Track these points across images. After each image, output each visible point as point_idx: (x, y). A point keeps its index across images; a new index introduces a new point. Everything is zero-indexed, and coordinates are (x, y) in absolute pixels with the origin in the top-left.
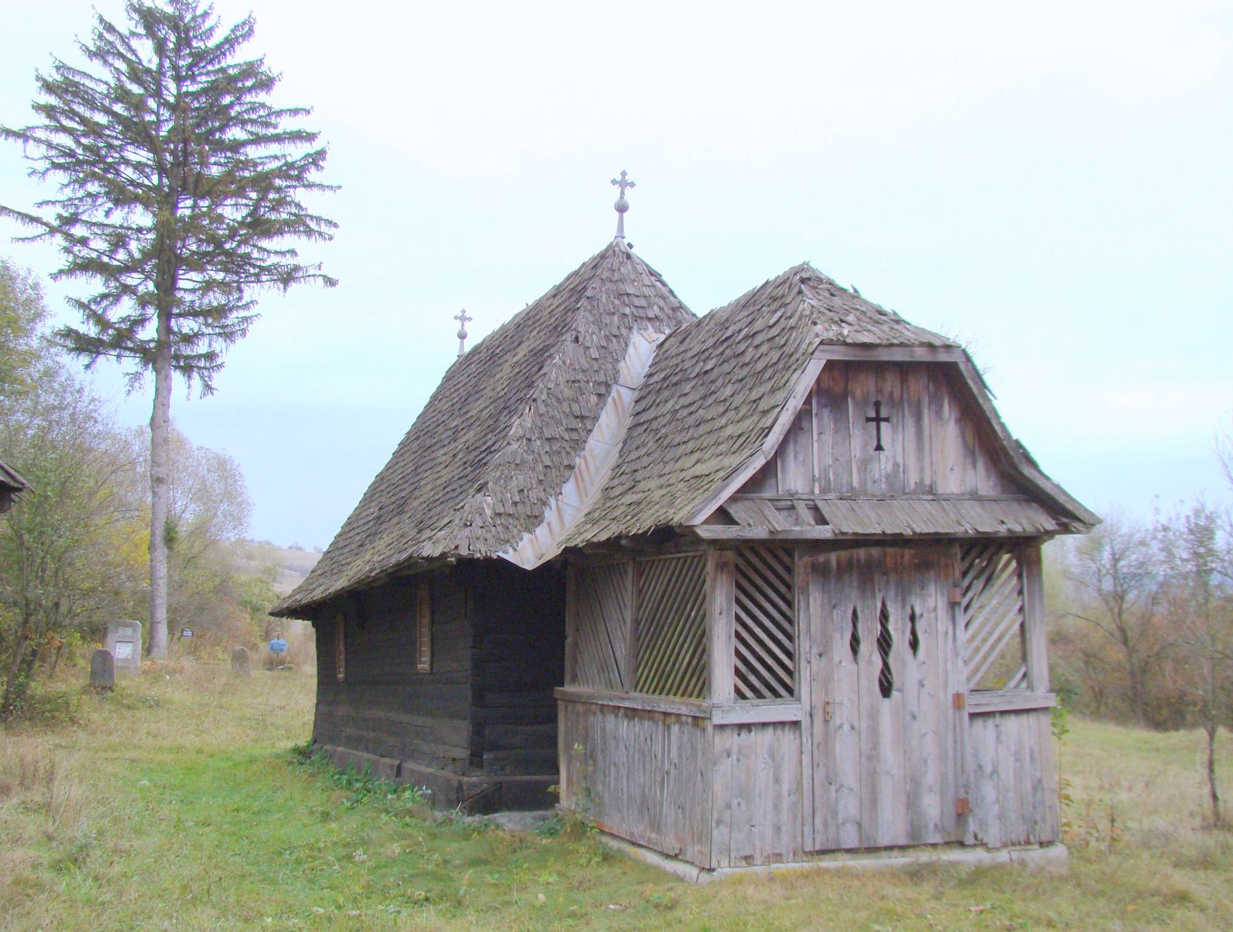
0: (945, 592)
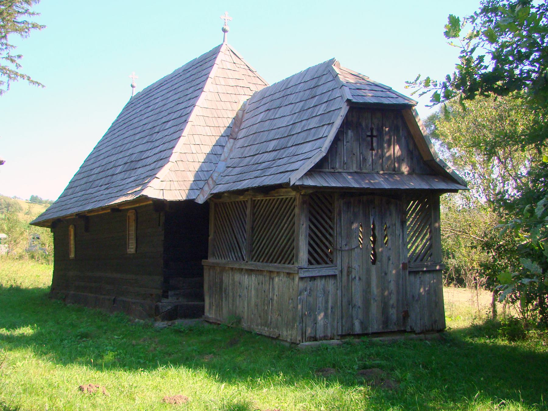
0: (399, 216)
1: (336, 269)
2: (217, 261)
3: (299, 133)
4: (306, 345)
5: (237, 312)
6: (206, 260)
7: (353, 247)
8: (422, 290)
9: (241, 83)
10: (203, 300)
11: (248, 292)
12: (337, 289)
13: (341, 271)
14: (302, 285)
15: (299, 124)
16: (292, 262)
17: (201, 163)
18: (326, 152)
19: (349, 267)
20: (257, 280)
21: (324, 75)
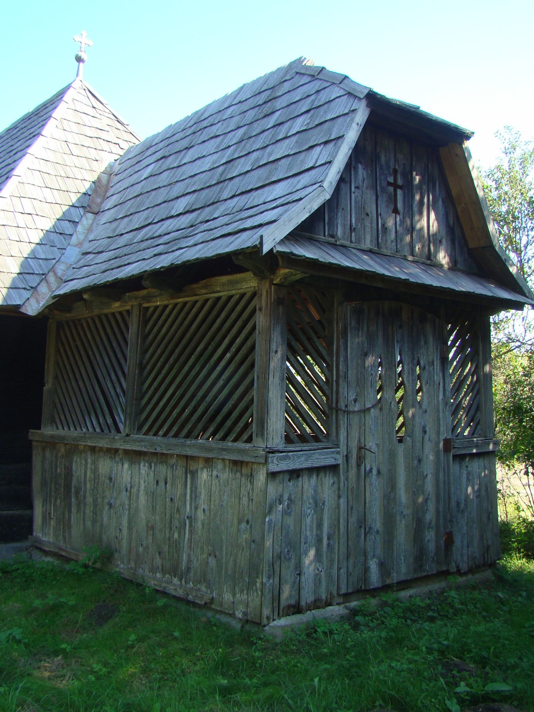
1: (338, 453)
2: (61, 432)
3: (248, 172)
4: (282, 627)
5: (105, 537)
6: (38, 431)
7: (368, 405)
8: (469, 490)
9: (103, 135)
10: (31, 507)
11: (130, 499)
12: (339, 497)
13: (347, 456)
14: (273, 490)
15: (243, 159)
16: (245, 437)
17: (33, 246)
18: (331, 193)
19: (360, 448)
20: (152, 474)
21: (285, 81)
